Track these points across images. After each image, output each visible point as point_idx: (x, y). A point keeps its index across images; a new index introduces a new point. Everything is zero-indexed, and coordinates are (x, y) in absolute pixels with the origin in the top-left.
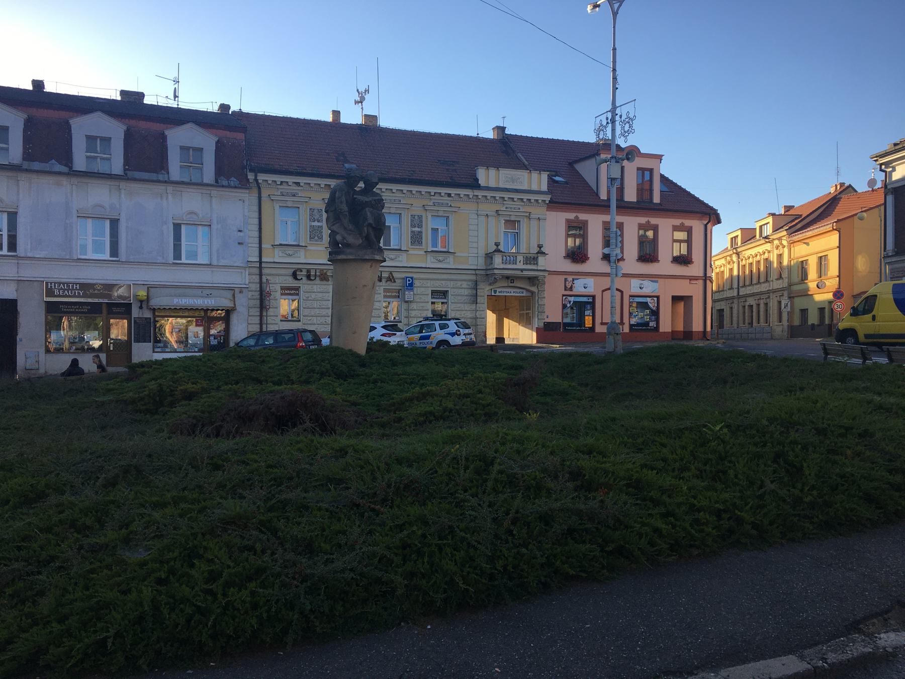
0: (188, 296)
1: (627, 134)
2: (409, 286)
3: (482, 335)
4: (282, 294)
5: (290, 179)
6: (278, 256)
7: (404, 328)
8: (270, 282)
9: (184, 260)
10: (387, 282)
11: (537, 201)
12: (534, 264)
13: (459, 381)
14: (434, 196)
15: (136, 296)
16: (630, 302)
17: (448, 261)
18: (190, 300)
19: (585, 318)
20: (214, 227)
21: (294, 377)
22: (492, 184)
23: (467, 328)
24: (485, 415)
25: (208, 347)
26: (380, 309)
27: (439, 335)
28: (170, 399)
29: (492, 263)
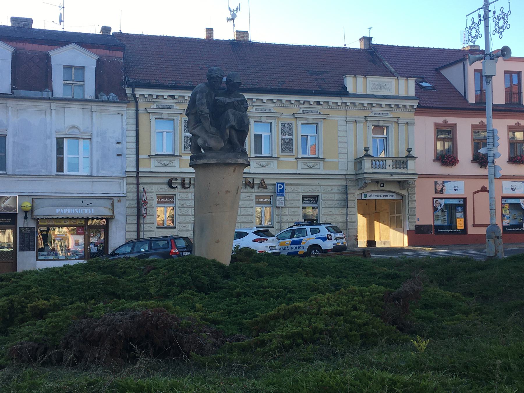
0: (70, 206)
1: (501, 30)
2: (280, 192)
3: (353, 239)
4: (158, 202)
5: (166, 93)
6: (154, 166)
7: (276, 233)
8: (146, 191)
9: (66, 172)
10: (258, 188)
11: (405, 106)
12: (404, 168)
13: (330, 295)
14: (303, 104)
15: (21, 207)
16: (502, 204)
17: (318, 167)
18: (71, 210)
19: (456, 220)
20: (94, 140)
21: (152, 290)
22: (360, 91)
23: (338, 233)
24: (361, 336)
25: (88, 255)
26: (252, 215)
27: (310, 240)
28: (21, 316)
29: (362, 168)
